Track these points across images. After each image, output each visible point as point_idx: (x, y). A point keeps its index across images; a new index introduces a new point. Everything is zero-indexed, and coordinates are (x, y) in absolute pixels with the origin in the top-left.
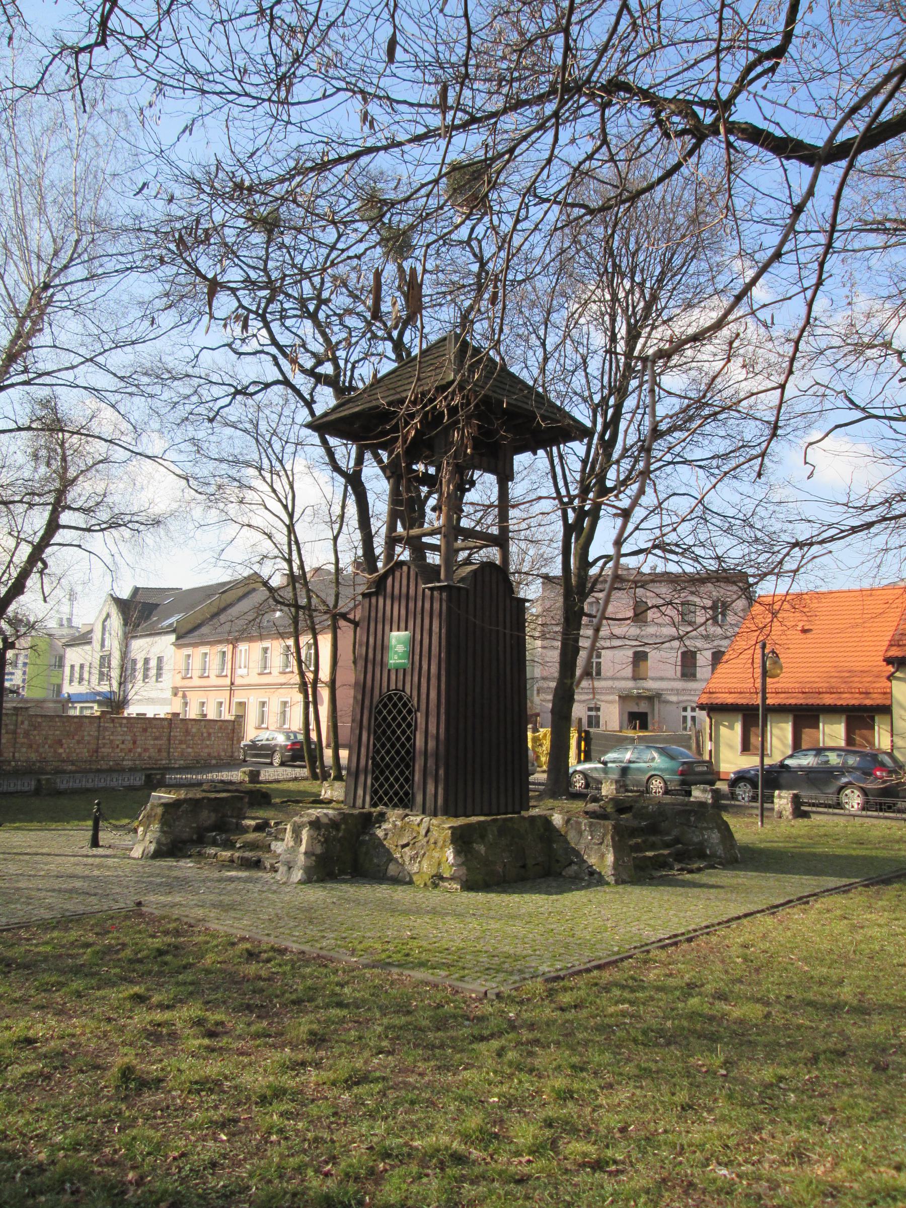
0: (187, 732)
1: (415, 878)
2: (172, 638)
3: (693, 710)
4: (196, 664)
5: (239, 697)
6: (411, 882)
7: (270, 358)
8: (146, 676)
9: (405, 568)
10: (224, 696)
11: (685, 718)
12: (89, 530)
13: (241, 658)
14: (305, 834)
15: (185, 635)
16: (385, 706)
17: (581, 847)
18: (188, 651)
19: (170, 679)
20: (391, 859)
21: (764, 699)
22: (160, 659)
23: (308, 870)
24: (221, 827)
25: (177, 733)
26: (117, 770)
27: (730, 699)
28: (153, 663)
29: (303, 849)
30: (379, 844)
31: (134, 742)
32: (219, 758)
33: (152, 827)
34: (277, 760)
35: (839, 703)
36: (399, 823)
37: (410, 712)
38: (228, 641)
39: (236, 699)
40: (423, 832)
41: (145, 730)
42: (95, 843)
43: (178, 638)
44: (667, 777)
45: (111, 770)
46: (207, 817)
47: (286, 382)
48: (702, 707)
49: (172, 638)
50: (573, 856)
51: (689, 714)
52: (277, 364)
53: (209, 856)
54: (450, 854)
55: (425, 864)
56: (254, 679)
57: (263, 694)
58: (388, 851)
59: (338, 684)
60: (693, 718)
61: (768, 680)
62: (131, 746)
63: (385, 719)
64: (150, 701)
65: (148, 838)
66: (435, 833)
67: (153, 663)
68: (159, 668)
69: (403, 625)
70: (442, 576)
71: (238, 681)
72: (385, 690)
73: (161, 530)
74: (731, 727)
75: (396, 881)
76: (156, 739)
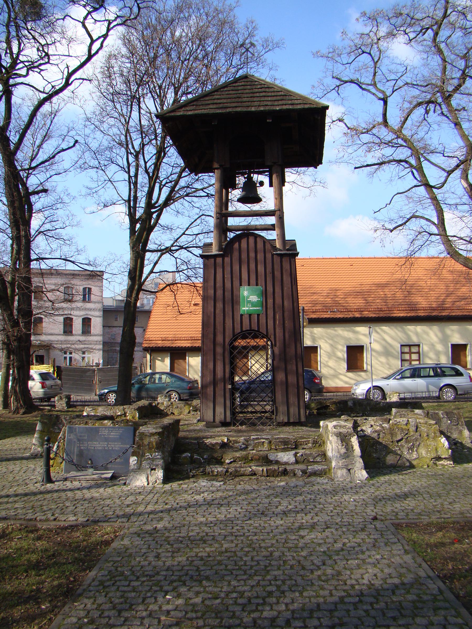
1: (414, 463)
6: (412, 466)
9: (251, 240)
27: (160, 344)
36: (385, 425)
44: (179, 391)
55: (423, 452)
58: (386, 447)
60: (71, 358)
74: (163, 361)
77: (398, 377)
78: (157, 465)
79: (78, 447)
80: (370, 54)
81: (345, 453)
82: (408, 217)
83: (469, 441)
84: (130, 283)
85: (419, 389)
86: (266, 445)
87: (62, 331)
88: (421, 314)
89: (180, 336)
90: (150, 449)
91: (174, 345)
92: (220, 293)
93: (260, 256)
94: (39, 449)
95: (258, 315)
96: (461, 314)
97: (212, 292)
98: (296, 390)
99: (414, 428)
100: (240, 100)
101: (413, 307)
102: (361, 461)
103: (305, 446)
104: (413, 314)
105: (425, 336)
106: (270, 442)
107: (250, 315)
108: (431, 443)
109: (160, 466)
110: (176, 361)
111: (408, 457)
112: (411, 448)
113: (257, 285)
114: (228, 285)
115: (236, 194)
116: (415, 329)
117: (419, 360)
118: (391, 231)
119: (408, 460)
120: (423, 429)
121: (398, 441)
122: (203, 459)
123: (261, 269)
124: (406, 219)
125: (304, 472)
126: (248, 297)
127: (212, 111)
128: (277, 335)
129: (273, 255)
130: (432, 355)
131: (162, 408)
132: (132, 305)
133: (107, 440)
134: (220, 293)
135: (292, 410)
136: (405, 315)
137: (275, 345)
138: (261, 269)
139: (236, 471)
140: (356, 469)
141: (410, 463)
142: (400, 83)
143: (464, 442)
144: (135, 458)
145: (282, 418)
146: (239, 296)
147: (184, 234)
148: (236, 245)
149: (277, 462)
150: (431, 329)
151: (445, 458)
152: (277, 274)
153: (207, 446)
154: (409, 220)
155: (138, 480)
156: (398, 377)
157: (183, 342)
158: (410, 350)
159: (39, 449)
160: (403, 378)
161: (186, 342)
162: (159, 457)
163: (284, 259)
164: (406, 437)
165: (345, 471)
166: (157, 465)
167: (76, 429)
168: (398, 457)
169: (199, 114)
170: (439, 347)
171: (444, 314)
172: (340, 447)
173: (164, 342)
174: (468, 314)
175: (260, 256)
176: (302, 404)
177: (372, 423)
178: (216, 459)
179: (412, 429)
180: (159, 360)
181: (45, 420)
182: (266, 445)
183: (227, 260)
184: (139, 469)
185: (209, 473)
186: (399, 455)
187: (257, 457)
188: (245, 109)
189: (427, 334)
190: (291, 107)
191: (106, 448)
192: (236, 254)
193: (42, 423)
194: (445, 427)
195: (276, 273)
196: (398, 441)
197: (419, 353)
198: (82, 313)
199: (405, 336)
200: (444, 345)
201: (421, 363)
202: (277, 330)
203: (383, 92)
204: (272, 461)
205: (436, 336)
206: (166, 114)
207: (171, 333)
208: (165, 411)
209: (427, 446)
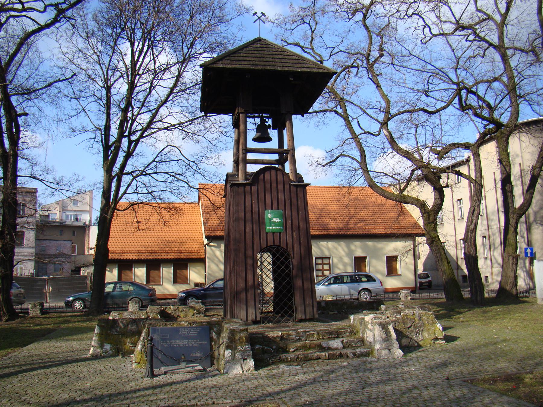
1: (421, 343)
6: (419, 346)
35: (143, 258)
36: (399, 316)
44: (142, 298)
55: (426, 335)
69: (275, 205)
74: (111, 271)
77: (327, 283)
78: (248, 356)
79: (161, 345)
80: (309, 24)
81: (386, 337)
82: (337, 155)
84: (104, 202)
85: (343, 293)
86: (315, 336)
88: (332, 232)
89: (127, 249)
90: (241, 343)
91: (122, 258)
92: (248, 216)
93: (280, 187)
94: (99, 350)
95: (280, 233)
96: (362, 232)
97: (243, 214)
98: (311, 293)
99: (418, 318)
100: (264, 60)
101: (325, 227)
102: (397, 343)
103: (344, 335)
104: (325, 233)
105: (335, 251)
106: (318, 333)
107: (273, 233)
109: (251, 357)
110: (123, 272)
111: (416, 339)
112: (418, 333)
113: (278, 209)
114: (255, 209)
115: (252, 134)
116: (327, 245)
117: (330, 270)
118: (324, 166)
119: (416, 342)
120: (424, 318)
121: (409, 328)
122: (273, 349)
123: (281, 196)
124: (335, 157)
125: (354, 354)
126: (272, 219)
127: (247, 67)
128: (295, 249)
129: (290, 185)
130: (341, 266)
131: (170, 312)
132: (108, 221)
133: (188, 338)
134: (248, 216)
135: (308, 310)
136: (319, 233)
137: (294, 258)
138: (281, 196)
139: (305, 357)
140: (394, 349)
141: (418, 343)
142: (336, 50)
144: (230, 351)
145: (300, 316)
146: (264, 218)
148: (262, 177)
149: (329, 349)
150: (339, 245)
151: (440, 339)
152: (294, 200)
153: (270, 339)
154: (337, 158)
155: (234, 369)
156: (327, 283)
157: (130, 254)
158: (322, 262)
159: (99, 350)
160: (330, 284)
161: (133, 254)
162: (249, 349)
163: (299, 189)
165: (387, 351)
166: (248, 356)
167: (158, 330)
169: (244, 69)
170: (346, 260)
171: (349, 233)
172: (382, 333)
174: (367, 232)
175: (280, 187)
176: (315, 304)
177: (389, 315)
178: (282, 348)
179: (417, 318)
180: (108, 271)
181: (103, 324)
182: (315, 336)
183: (254, 188)
184: (233, 361)
185: (284, 360)
187: (314, 346)
188: (273, 68)
189: (337, 249)
190: (308, 70)
191: (187, 345)
192: (261, 184)
193: (100, 326)
195: (292, 199)
196: (409, 328)
197: (329, 264)
199: (319, 251)
200: (349, 258)
201: (331, 273)
202: (295, 245)
203: (320, 56)
204: (325, 348)
205: (344, 250)
206: (209, 65)
208: (172, 314)
209: (428, 330)
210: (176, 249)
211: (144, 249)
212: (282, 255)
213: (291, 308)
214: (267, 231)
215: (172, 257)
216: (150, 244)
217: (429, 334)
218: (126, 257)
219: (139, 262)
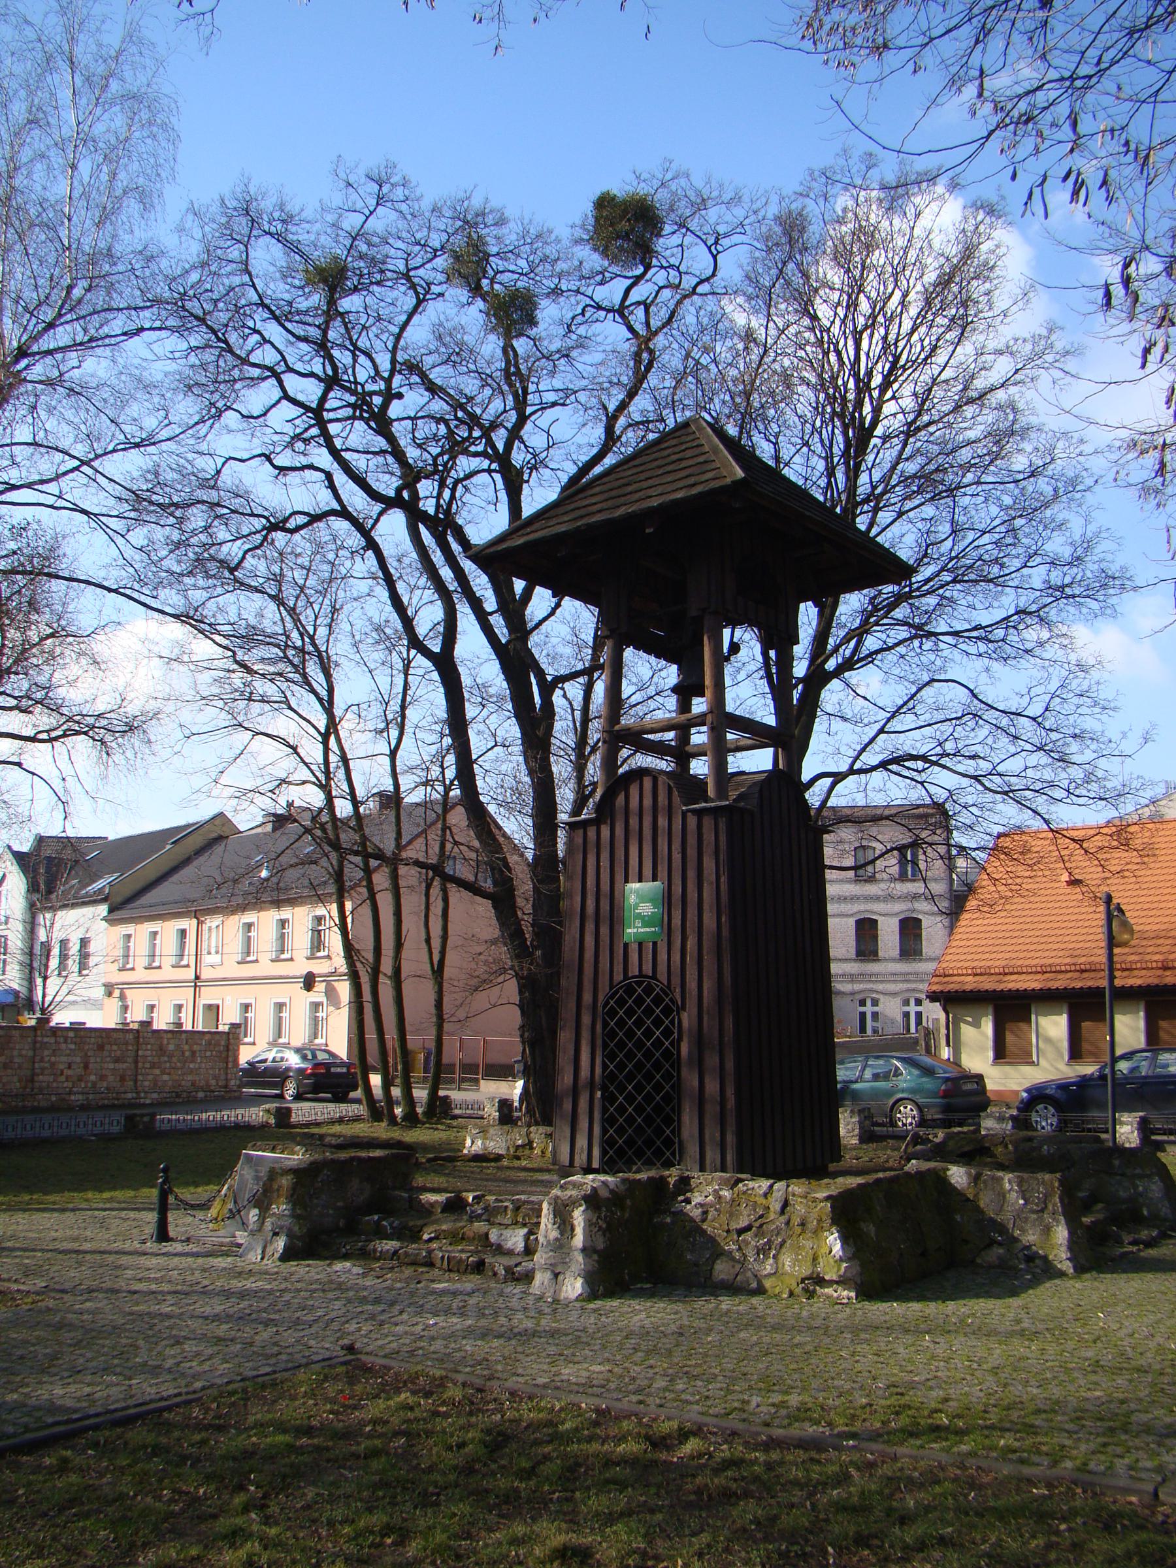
0: (162, 1050)
1: (768, 1284)
2: (103, 909)
3: (918, 1002)
4: (140, 945)
5: (209, 996)
6: (760, 1291)
7: (323, 476)
8: (62, 965)
9: (647, 782)
10: (185, 995)
11: (863, 1015)
12: (33, 739)
13: (211, 940)
14: (579, 1216)
15: (123, 906)
16: (621, 1002)
17: (1007, 1217)
18: (129, 929)
19: (103, 970)
20: (718, 1253)
21: (1112, 978)
22: (84, 942)
23: (591, 1279)
24: (382, 1204)
25: (146, 1052)
26: (60, 1108)
27: (970, 983)
28: (74, 948)
29: (579, 1240)
30: (693, 1230)
31: (86, 1067)
32: (207, 1089)
33: (274, 1208)
34: (290, 1090)
35: (1054, 985)
36: (726, 1193)
37: (667, 1011)
38: (196, 915)
39: (204, 1000)
40: (778, 1206)
41: (101, 1047)
42: (163, 1235)
43: (111, 911)
44: (921, 1101)
45: (53, 1109)
46: (358, 1190)
47: (344, 513)
48: (933, 997)
49: (103, 909)
50: (992, 1232)
51: (913, 1009)
52: (332, 486)
53: (383, 1256)
54: (834, 1242)
55: (787, 1260)
56: (233, 970)
57: (272, 988)
58: (712, 1240)
59: (403, 976)
60: (919, 1015)
61: (1116, 951)
62: (80, 1071)
63: (621, 1023)
64: (80, 1003)
65: (268, 1225)
66: (799, 1208)
67: (74, 948)
68: (84, 956)
69: (648, 871)
70: (711, 792)
71: (206, 974)
72: (619, 976)
73: (136, 740)
74: (977, 1025)
75: (733, 1288)
76: (117, 1060)
81: (556, 1239)
83: (1064, 1256)
87: (852, 953)
89: (1020, 963)
108: (807, 1243)
112: (763, 1251)
113: (654, 879)
140: (568, 1274)
141: (760, 1283)
143: (1051, 1257)
147: (881, 731)
164: (757, 1224)
165: (548, 1275)
168: (738, 1267)
173: (981, 978)
180: (968, 1023)
186: (738, 1261)
194: (1010, 1216)
198: (899, 907)
207: (1000, 956)
210: (1157, 957)
211: (1068, 960)
212: (658, 1001)
213: (669, 1143)
214: (626, 939)
215: (1136, 982)
216: (1088, 945)
217: (795, 1261)
218: (1012, 986)
219: (1049, 998)
